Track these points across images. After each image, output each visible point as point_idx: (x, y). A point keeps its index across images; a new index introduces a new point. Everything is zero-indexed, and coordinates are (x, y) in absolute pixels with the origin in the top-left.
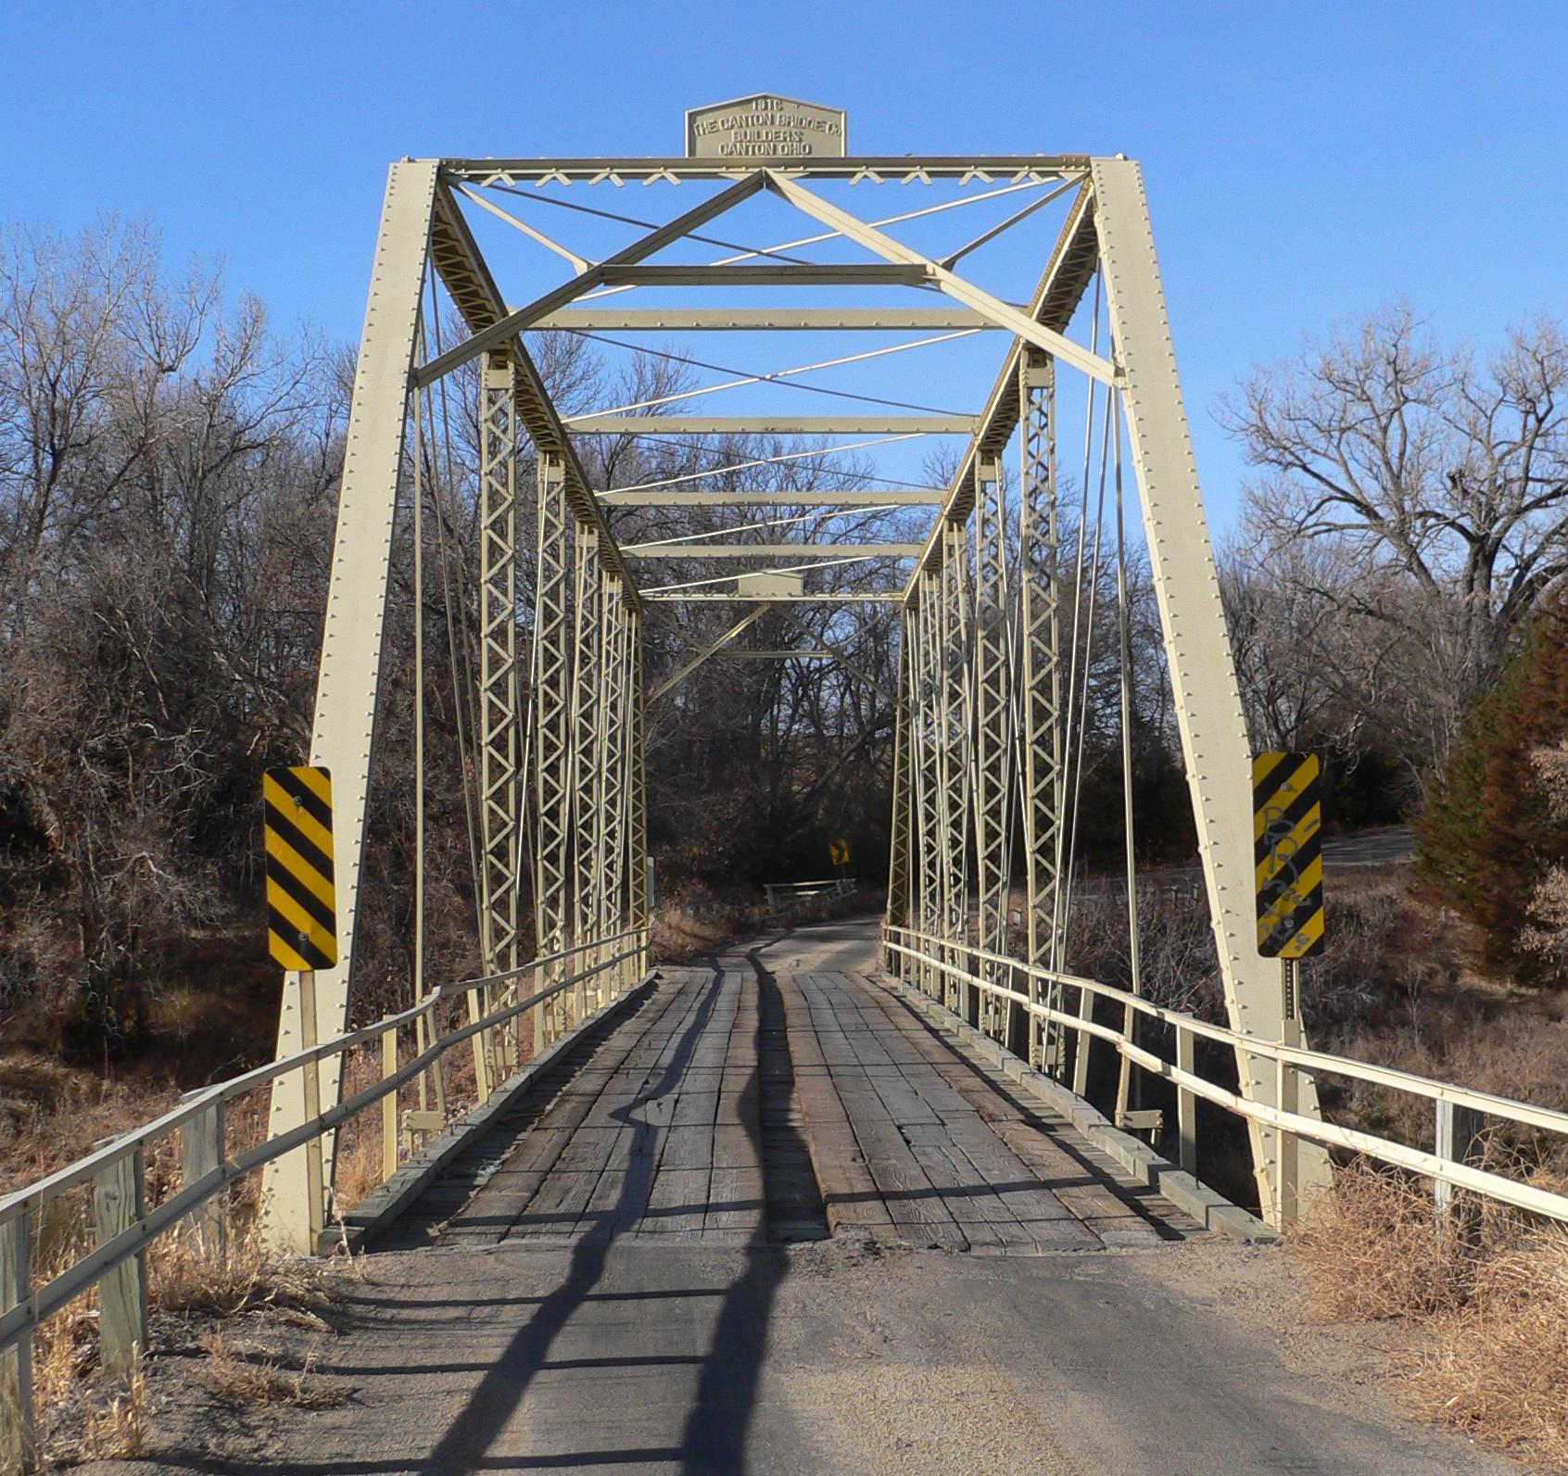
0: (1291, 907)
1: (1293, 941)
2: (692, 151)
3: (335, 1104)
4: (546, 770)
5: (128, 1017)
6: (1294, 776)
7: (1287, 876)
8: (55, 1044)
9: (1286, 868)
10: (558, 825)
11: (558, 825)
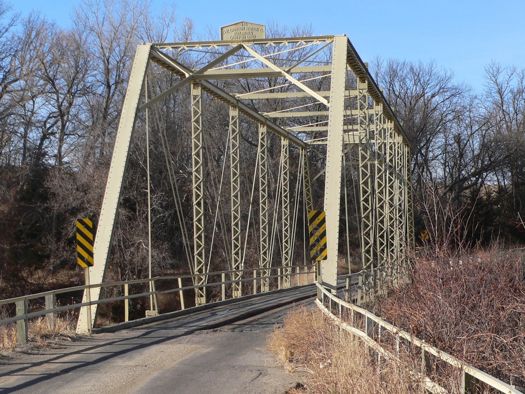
0: (319, 248)
1: (320, 257)
2: (222, 38)
3: (98, 300)
4: (364, 200)
5: (139, 303)
6: (320, 216)
7: (318, 241)
8: (110, 314)
9: (318, 239)
10: (384, 226)
11: (384, 226)
